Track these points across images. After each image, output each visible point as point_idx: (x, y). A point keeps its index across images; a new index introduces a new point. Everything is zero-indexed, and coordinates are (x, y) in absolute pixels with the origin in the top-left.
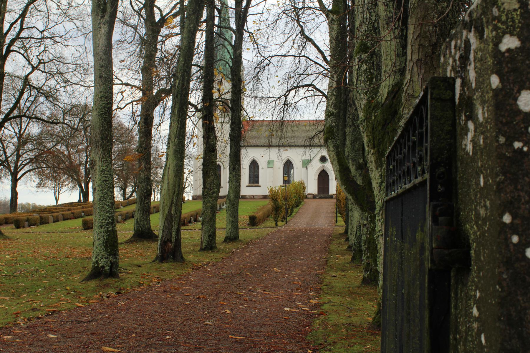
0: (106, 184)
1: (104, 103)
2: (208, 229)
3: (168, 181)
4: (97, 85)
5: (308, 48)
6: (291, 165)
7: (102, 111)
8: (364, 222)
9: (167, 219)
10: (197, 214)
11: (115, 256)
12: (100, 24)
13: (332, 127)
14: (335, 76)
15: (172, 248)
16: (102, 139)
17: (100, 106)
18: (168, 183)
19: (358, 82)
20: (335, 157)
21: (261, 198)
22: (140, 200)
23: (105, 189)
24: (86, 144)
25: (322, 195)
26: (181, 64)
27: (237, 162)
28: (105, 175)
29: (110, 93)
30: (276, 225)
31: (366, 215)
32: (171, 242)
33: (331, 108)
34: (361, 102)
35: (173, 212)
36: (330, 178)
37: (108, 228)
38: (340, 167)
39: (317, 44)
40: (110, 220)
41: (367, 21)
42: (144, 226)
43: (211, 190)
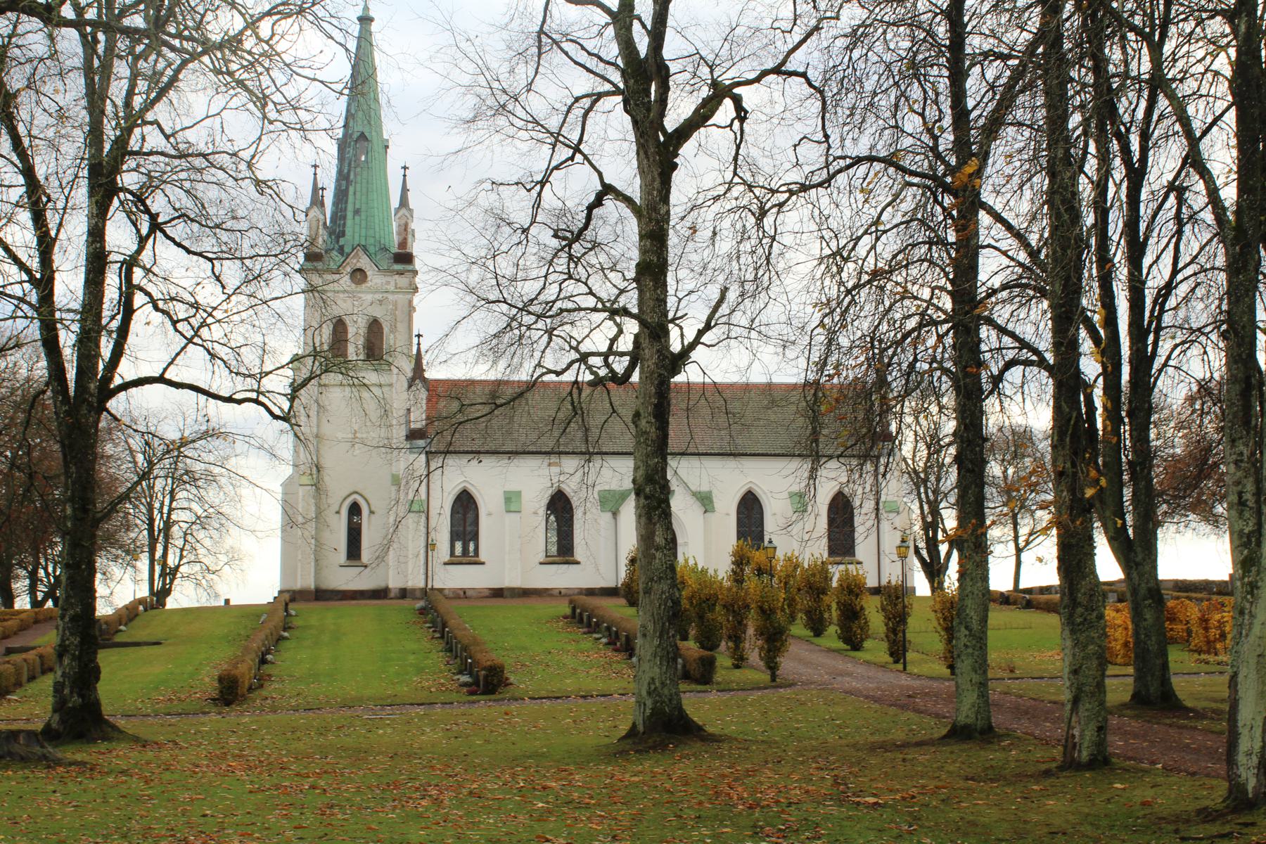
2: (1095, 712)
21: (487, 597)
22: (658, 627)
24: (51, 442)
43: (1093, 610)
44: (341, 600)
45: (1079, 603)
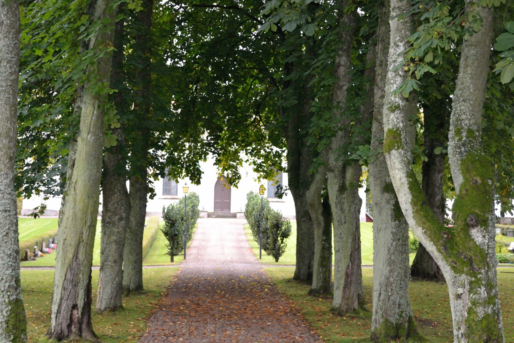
10: (43, 241)
14: (400, 44)
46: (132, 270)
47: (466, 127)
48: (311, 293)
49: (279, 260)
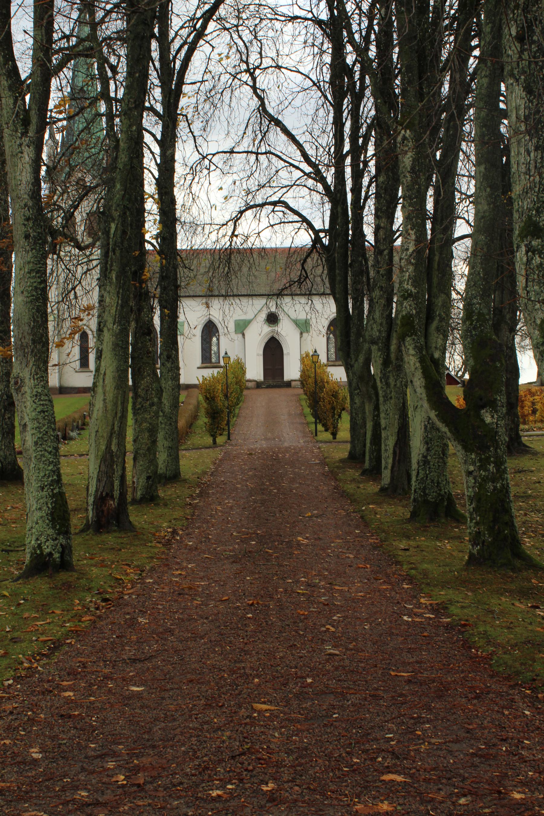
0: (44, 418)
1: (35, 282)
3: (105, 396)
4: (21, 250)
5: (271, 136)
6: (214, 330)
7: (33, 296)
8: (468, 468)
9: (103, 460)
10: (66, 425)
11: (67, 535)
12: (20, 145)
13: (411, 316)
14: (410, 232)
15: (115, 508)
16: (34, 341)
17: (29, 287)
18: (104, 400)
19: (529, 283)
20: (418, 365)
23: (44, 425)
25: (271, 382)
26: (118, 196)
27: (173, 345)
28: (42, 403)
29: (43, 264)
30: (215, 442)
31: (473, 456)
32: (112, 497)
33: (408, 284)
34: (535, 314)
35: (114, 448)
36: (285, 352)
37: (52, 490)
38: (426, 380)
39: (289, 127)
40: (55, 477)
41: (535, 187)
42: (5, 458)
43: (147, 400)
44: (77, 393)
45: (139, 396)
46: (168, 457)
47: (476, 311)
48: (364, 473)
49: (338, 436)
